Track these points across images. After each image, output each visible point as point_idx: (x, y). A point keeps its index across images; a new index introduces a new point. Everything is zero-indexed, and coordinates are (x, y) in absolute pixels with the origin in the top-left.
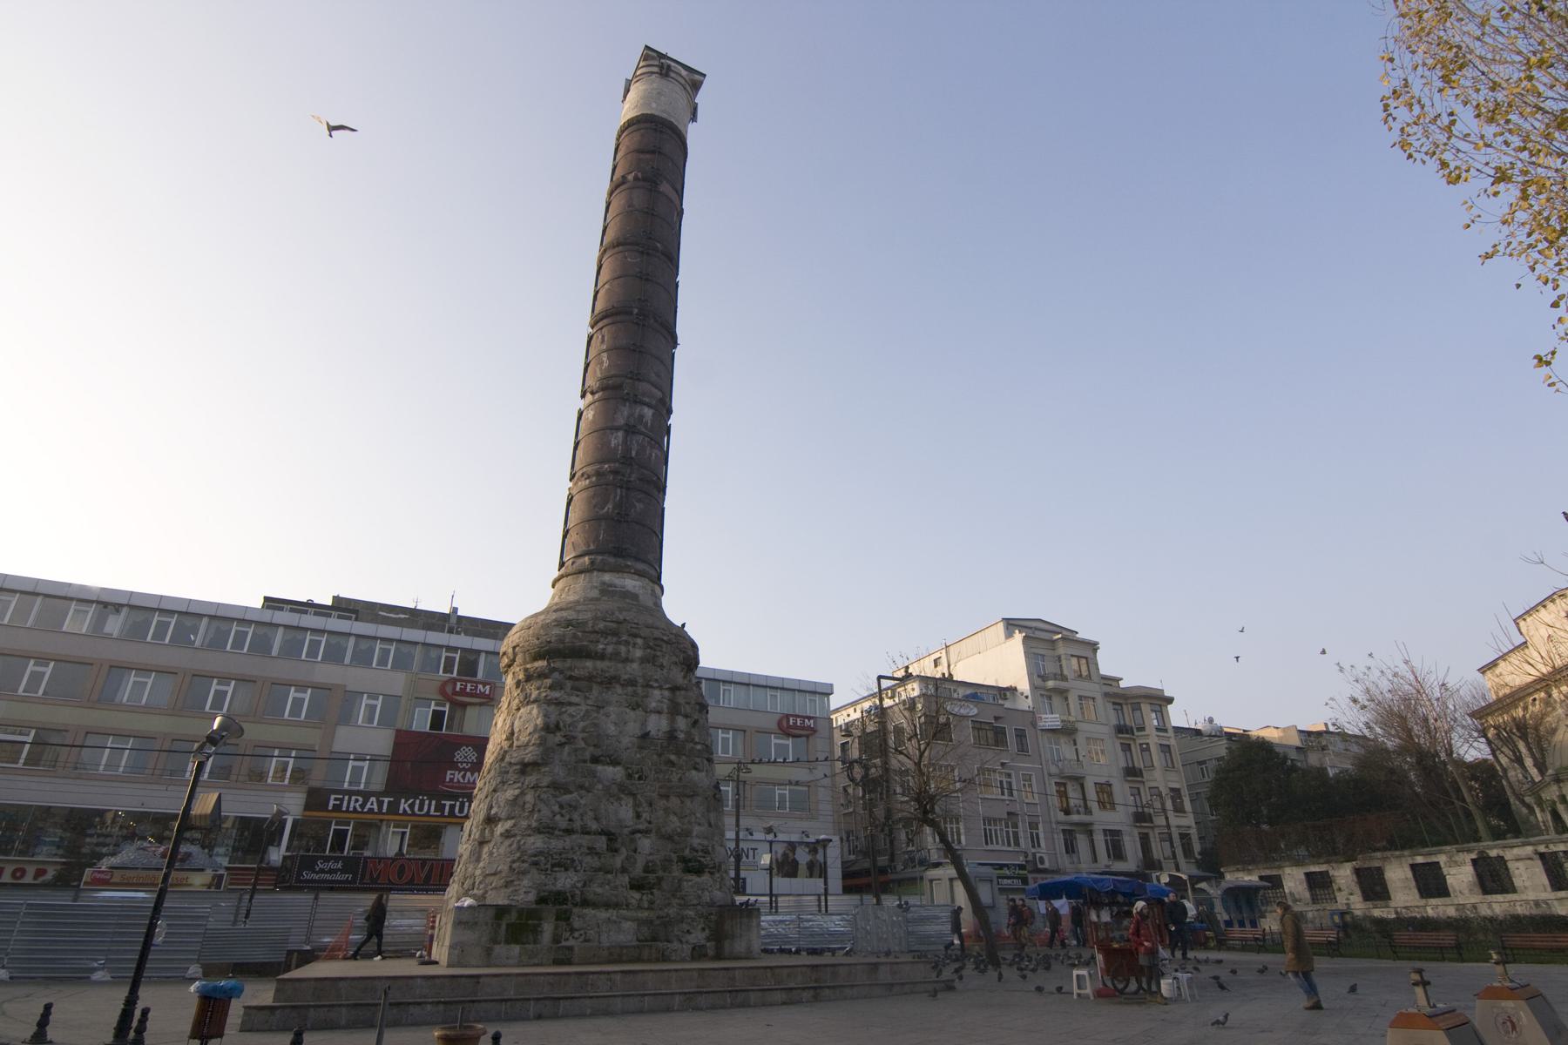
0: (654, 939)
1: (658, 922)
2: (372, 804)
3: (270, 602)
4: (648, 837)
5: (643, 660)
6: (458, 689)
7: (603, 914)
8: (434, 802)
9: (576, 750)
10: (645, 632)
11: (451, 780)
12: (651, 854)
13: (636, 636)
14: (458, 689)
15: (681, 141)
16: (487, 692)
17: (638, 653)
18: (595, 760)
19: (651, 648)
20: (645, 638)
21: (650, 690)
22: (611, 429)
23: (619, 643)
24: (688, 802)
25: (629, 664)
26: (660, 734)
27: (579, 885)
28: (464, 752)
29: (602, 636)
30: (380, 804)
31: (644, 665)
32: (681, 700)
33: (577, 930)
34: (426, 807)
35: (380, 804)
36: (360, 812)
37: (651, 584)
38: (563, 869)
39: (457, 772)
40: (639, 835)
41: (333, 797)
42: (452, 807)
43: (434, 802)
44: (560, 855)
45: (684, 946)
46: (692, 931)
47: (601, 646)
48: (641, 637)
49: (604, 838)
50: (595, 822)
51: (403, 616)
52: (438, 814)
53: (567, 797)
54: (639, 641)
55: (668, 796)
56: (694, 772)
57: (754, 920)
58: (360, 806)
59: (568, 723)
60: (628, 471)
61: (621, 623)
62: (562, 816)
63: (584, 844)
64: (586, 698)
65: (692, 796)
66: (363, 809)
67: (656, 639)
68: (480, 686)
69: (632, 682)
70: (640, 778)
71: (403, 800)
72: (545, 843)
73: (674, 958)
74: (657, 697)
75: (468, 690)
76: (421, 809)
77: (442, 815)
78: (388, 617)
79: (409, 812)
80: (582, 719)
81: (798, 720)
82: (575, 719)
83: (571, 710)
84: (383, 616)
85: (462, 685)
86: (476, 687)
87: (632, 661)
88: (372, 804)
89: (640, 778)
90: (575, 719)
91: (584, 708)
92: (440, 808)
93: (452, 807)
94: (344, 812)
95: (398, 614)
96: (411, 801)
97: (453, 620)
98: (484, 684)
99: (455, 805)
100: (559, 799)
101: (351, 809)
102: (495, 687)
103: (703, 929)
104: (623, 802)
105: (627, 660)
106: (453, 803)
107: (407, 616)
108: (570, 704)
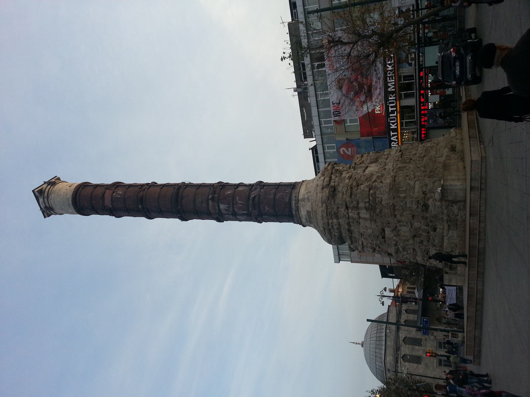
0: (457, 225)
2: (394, 138)
3: (307, 134)
4: (414, 223)
5: (337, 218)
7: (446, 240)
8: (391, 115)
9: (381, 244)
11: (379, 111)
12: (421, 223)
13: (328, 223)
15: (80, 188)
17: (335, 221)
18: (384, 237)
19: (331, 217)
23: (333, 228)
24: (397, 208)
25: (340, 223)
27: (434, 248)
30: (393, 135)
31: (339, 218)
32: (352, 205)
33: (452, 250)
34: (392, 101)
35: (393, 135)
37: (299, 202)
38: (429, 252)
39: (376, 109)
40: (413, 226)
42: (392, 107)
43: (391, 115)
44: (423, 253)
45: (459, 214)
46: (453, 211)
47: (336, 234)
49: (416, 239)
50: (409, 241)
51: (304, 111)
53: (400, 249)
54: (330, 221)
55: (395, 215)
56: (383, 203)
57: (448, 187)
58: (395, 143)
59: (370, 245)
60: (253, 214)
61: (324, 229)
62: (408, 251)
63: (418, 245)
64: (359, 239)
65: (394, 206)
66: (397, 141)
67: (327, 215)
69: (349, 224)
70: (389, 224)
71: (391, 127)
73: (464, 218)
74: (352, 214)
77: (396, 110)
78: (306, 116)
79: (396, 124)
83: (365, 244)
84: (307, 118)
87: (339, 222)
88: (394, 138)
89: (389, 224)
92: (393, 112)
93: (392, 107)
96: (391, 124)
97: (300, 90)
99: (391, 106)
100: (402, 251)
103: (452, 206)
104: (399, 229)
105: (339, 224)
106: (390, 107)
108: (362, 244)
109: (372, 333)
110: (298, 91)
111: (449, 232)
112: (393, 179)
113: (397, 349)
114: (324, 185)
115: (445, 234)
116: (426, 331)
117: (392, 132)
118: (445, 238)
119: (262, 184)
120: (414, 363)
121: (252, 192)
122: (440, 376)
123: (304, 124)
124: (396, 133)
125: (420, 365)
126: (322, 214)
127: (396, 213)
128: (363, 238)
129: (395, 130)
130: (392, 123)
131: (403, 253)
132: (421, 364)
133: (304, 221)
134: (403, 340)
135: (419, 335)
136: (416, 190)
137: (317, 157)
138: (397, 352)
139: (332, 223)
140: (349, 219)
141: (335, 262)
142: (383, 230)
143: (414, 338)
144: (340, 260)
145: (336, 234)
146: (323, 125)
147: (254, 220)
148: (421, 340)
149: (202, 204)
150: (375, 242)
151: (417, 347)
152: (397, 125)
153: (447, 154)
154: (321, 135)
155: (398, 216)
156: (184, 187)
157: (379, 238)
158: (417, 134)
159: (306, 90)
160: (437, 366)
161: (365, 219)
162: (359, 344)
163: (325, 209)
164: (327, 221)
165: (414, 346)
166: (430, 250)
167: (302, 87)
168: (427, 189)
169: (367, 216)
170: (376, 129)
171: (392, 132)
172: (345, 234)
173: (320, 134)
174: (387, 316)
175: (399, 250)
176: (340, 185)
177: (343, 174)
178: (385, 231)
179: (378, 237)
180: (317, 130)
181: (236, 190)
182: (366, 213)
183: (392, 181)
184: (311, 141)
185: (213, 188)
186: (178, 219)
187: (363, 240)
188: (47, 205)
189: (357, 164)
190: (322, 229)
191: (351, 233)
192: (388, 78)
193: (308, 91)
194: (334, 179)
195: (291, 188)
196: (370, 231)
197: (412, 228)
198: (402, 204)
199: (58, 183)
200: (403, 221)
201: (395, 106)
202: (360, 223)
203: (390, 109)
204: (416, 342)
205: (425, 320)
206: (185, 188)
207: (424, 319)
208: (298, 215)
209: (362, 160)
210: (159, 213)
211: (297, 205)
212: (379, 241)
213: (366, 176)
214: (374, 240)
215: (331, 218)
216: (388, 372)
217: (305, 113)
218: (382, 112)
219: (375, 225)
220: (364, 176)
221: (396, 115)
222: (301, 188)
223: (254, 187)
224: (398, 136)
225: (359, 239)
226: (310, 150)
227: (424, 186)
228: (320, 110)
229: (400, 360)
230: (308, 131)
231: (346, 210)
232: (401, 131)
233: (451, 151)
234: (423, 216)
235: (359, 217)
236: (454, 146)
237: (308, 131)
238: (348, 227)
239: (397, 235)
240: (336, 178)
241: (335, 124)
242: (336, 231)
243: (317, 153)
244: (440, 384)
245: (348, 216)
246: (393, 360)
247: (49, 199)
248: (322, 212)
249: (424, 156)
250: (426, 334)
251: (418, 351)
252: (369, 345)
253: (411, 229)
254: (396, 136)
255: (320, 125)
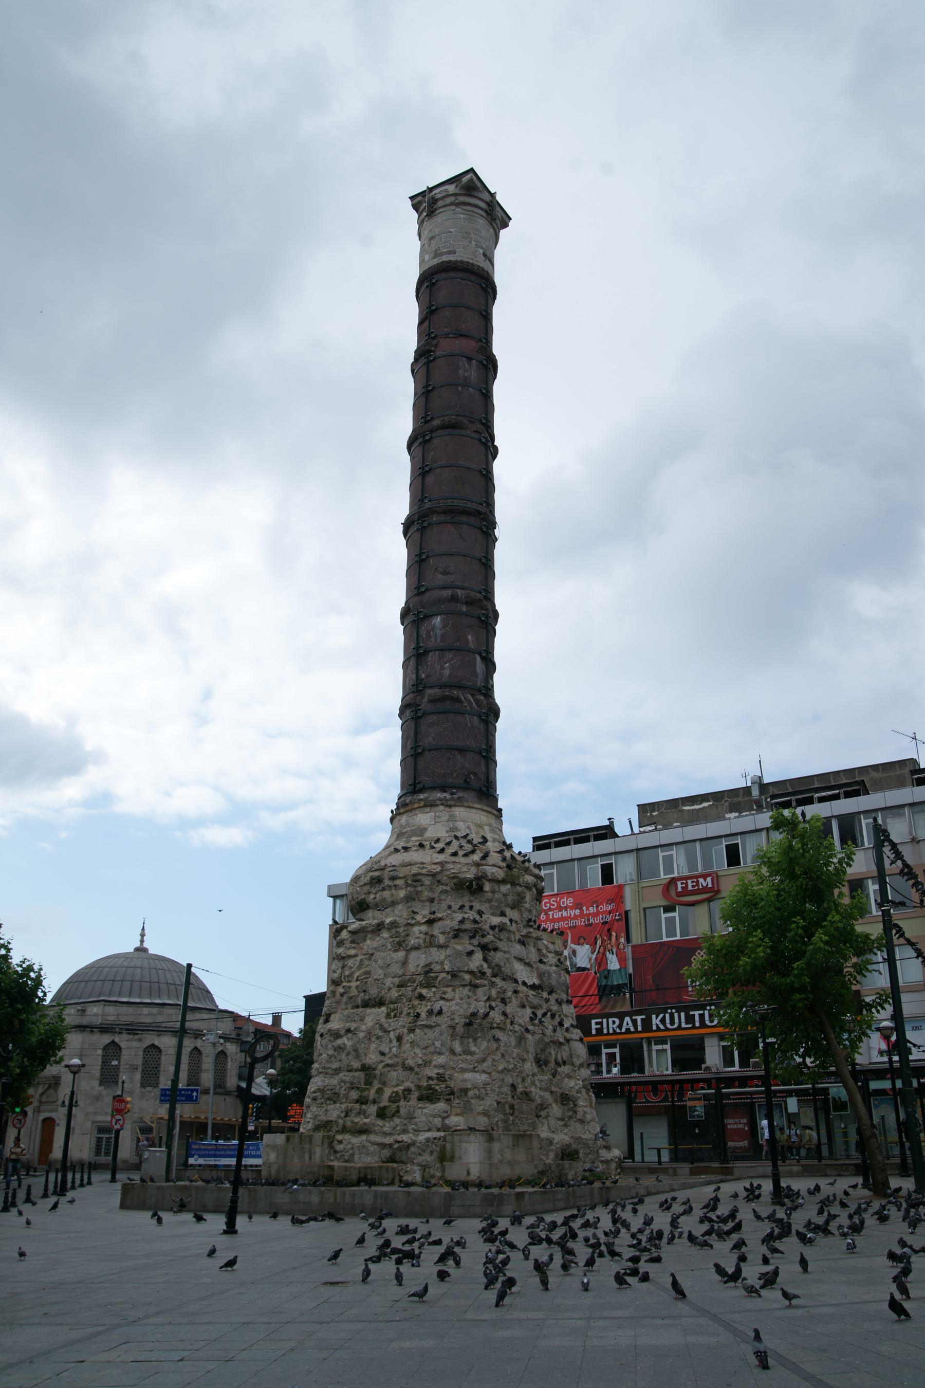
1: (396, 1146)
2: (628, 1024)
5: (409, 899)
6: (680, 889)
9: (351, 998)
10: (403, 872)
14: (680, 889)
16: (710, 885)
18: (366, 1004)
20: (404, 877)
21: (409, 927)
22: (442, 650)
23: (384, 889)
26: (419, 969)
27: (343, 1114)
28: (699, 956)
29: (371, 887)
30: (635, 1022)
31: (409, 904)
32: (436, 932)
35: (635, 1022)
36: (663, 1030)
37: (447, 809)
41: (593, 1021)
42: (702, 1017)
43: (683, 1014)
47: (372, 896)
48: (400, 878)
51: (706, 804)
52: (690, 1026)
54: (399, 882)
55: (414, 1030)
66: (621, 1029)
68: (701, 880)
71: (654, 1017)
72: (322, 1081)
75: (690, 888)
76: (672, 1022)
77: (694, 1027)
79: (662, 1027)
80: (359, 967)
81: (689, 882)
82: (353, 970)
83: (350, 963)
85: (682, 884)
86: (697, 882)
88: (628, 1024)
90: (353, 970)
91: (358, 958)
92: (690, 1019)
93: (702, 1017)
94: (655, 1031)
95: (700, 804)
96: (661, 1016)
98: (705, 877)
100: (334, 1044)
101: (611, 1031)
102: (718, 877)
106: (701, 1012)
107: (711, 803)
108: (350, 957)
109: (168, 975)
110: (753, 788)
111: (376, 1146)
112: (495, 1025)
113: (133, 1029)
114: (484, 867)
115: (372, 1137)
116: (168, 1095)
117: (642, 1019)
118: (364, 1137)
119: (491, 718)
120: (103, 1069)
121: (473, 695)
122: (74, 1128)
123: (674, 804)
124: (640, 1029)
125: (98, 1082)
126: (416, 864)
127: (417, 1031)
128: (363, 957)
129: (647, 1024)
130: (664, 1018)
131: (330, 1046)
132: (101, 1084)
133: (403, 819)
134: (153, 1045)
135: (165, 1082)
136: (468, 1075)
137: (586, 840)
138: (126, 1030)
139: (395, 886)
140: (405, 926)
141: (329, 887)
142: (381, 1003)
143: (158, 1071)
144: (335, 897)
145: (372, 896)
146: (661, 855)
147: (407, 697)
148: (154, 1087)
149: (441, 573)
150: (354, 984)
151: (138, 1076)
152: (658, 1029)
153: (555, 1141)
154: (638, 850)
155: (412, 1035)
156: (483, 527)
157: (362, 994)
158: (671, 1075)
159: (755, 807)
160: (97, 1122)
161: (405, 963)
162: (142, 941)
163: (426, 870)
164: (400, 876)
165: (140, 1069)
166: (338, 1105)
167: (763, 797)
168: (472, 1098)
169: (411, 968)
170: (651, 980)
171: (642, 1019)
172: (371, 918)
173: (639, 847)
174: (208, 1007)
175: (337, 1038)
176: (487, 905)
177: (513, 911)
178: (379, 1007)
179: (364, 991)
180: (652, 838)
181: (477, 655)
182: (418, 966)
183: (492, 1023)
184: (630, 822)
185: (482, 598)
186: (408, 513)
187: (358, 958)
188: (440, 203)
189: (539, 942)
190: (383, 864)
191: (373, 932)
192: (600, 1020)
193: (754, 812)
194: (499, 891)
195: (481, 788)
196: (378, 973)
197: (384, 1067)
198: (438, 1044)
199: (492, 225)
200: (400, 1046)
201: (703, 1024)
202: (396, 951)
203: (697, 1013)
204: (150, 1075)
205: (195, 1094)
206: (481, 529)
207: (197, 1093)
208: (416, 805)
209: (548, 954)
210: (420, 468)
211: (438, 802)
212: (357, 993)
213: (505, 964)
214: (358, 983)
215: (407, 885)
216: (80, 1008)
217: (701, 806)
218: (691, 993)
219: (392, 985)
220: (508, 959)
221: (683, 1025)
222: (479, 812)
223: (482, 698)
224: (633, 1033)
225: (361, 948)
226: (609, 819)
227: (477, 1093)
228: (698, 844)
229: (107, 1039)
230: (656, 813)
231: (426, 919)
232: (644, 1040)
233: (562, 1150)
234: (411, 1091)
235: (411, 949)
236: (576, 1156)
237: (656, 813)
238: (388, 924)
239: (369, 1034)
240: (501, 895)
241: (665, 882)
242: (378, 896)
243: (598, 838)
244: (57, 1128)
245: (412, 925)
246: (108, 1022)
247: (453, 207)
248: (423, 863)
249: (552, 1092)
250: (162, 1095)
251: (131, 1080)
252: (139, 964)
253: (383, 1064)
254: (632, 1029)
255: (662, 846)
